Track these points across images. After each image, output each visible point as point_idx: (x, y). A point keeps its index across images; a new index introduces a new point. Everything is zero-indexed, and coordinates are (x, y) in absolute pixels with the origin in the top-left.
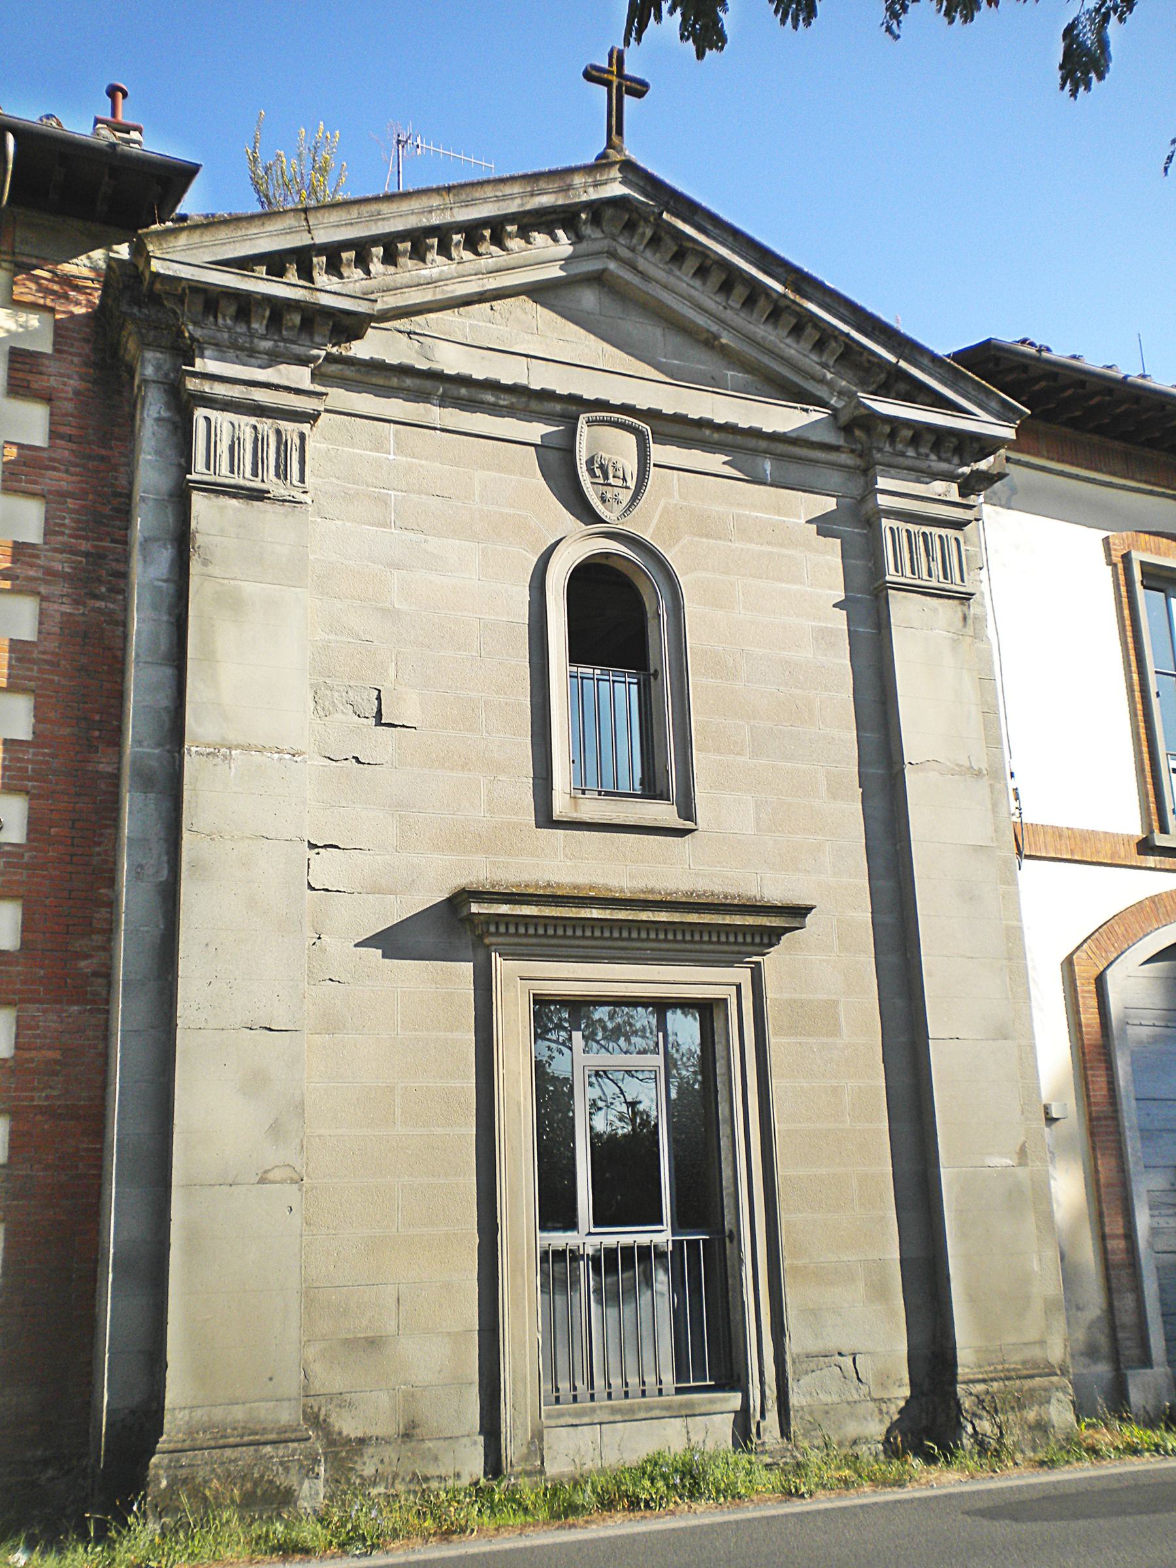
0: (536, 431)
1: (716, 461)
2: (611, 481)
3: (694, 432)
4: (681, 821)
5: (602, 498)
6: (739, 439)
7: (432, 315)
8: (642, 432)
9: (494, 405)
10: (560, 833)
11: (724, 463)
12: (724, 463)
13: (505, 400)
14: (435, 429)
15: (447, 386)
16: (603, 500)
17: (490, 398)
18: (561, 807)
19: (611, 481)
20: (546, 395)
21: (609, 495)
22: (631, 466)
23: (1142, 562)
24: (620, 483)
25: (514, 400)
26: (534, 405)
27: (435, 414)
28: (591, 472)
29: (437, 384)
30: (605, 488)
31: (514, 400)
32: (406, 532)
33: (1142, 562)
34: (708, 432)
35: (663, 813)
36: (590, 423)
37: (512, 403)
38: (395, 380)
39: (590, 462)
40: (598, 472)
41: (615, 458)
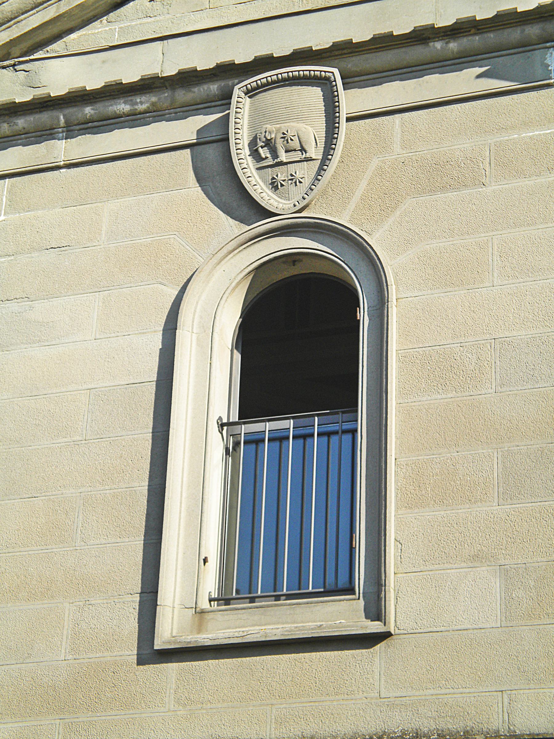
0: (187, 129)
1: (466, 80)
2: (283, 157)
3: (418, 53)
4: (369, 623)
5: (272, 183)
6: (492, 37)
7: (73, 36)
8: (327, 79)
9: (133, 114)
10: (173, 668)
11: (479, 76)
12: (479, 76)
13: (143, 103)
14: (58, 168)
15: (70, 111)
16: (274, 186)
17: (122, 107)
18: (170, 629)
19: (283, 157)
20: (188, 78)
21: (280, 177)
22: (313, 131)
23: (229, 113)
24: (298, 156)
25: (154, 99)
26: (183, 96)
27: (61, 149)
28: (255, 154)
29: (55, 113)
30: (276, 169)
31: (154, 99)
32: (8, 304)
33: (229, 113)
34: (438, 45)
35: (344, 615)
36: (251, 93)
37: (153, 104)
38: (5, 125)
39: (253, 144)
40: (264, 152)
41: (284, 127)
